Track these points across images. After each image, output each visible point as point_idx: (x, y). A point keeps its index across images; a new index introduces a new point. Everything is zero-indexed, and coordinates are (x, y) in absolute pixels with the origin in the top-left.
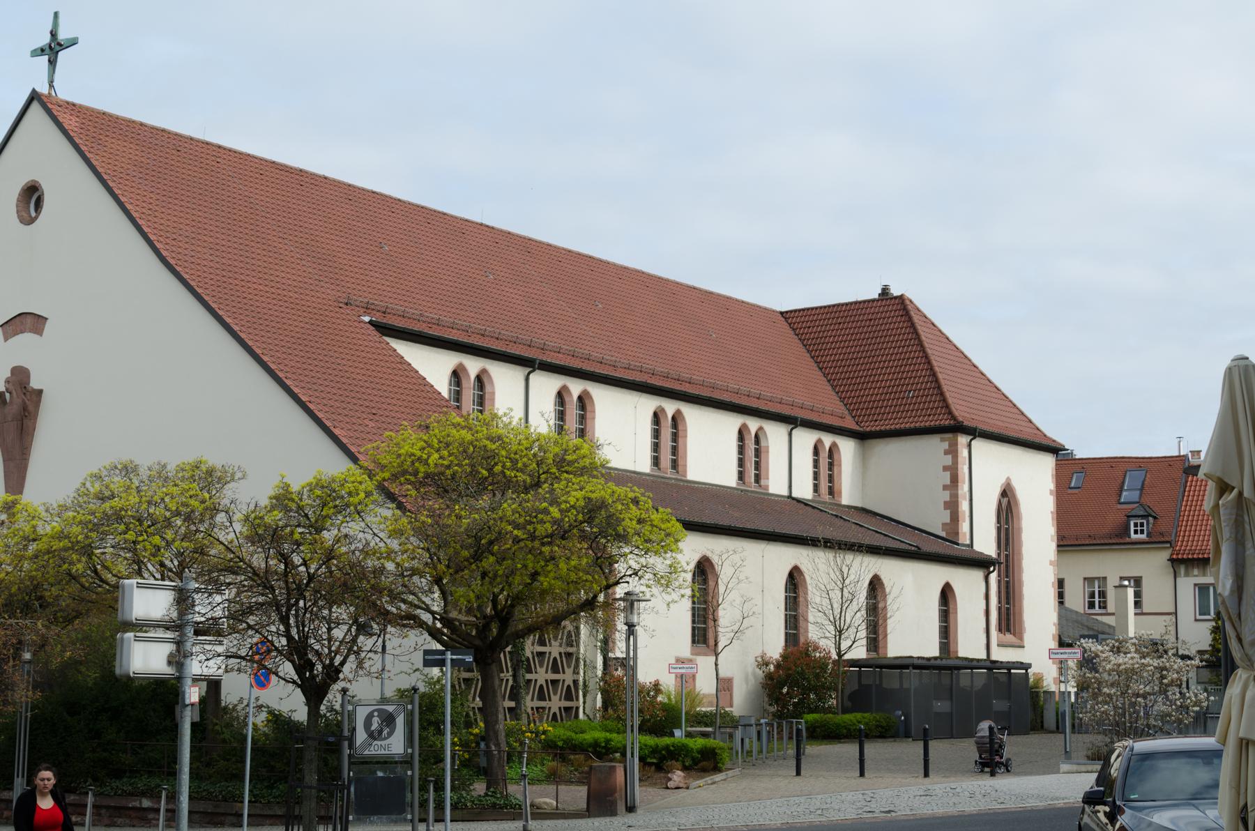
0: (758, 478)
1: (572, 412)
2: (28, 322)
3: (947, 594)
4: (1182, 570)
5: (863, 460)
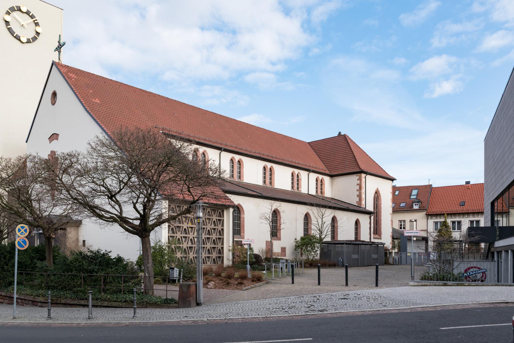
0: (298, 188)
1: (236, 166)
2: (54, 137)
3: (357, 223)
4: (430, 217)
5: (332, 183)
